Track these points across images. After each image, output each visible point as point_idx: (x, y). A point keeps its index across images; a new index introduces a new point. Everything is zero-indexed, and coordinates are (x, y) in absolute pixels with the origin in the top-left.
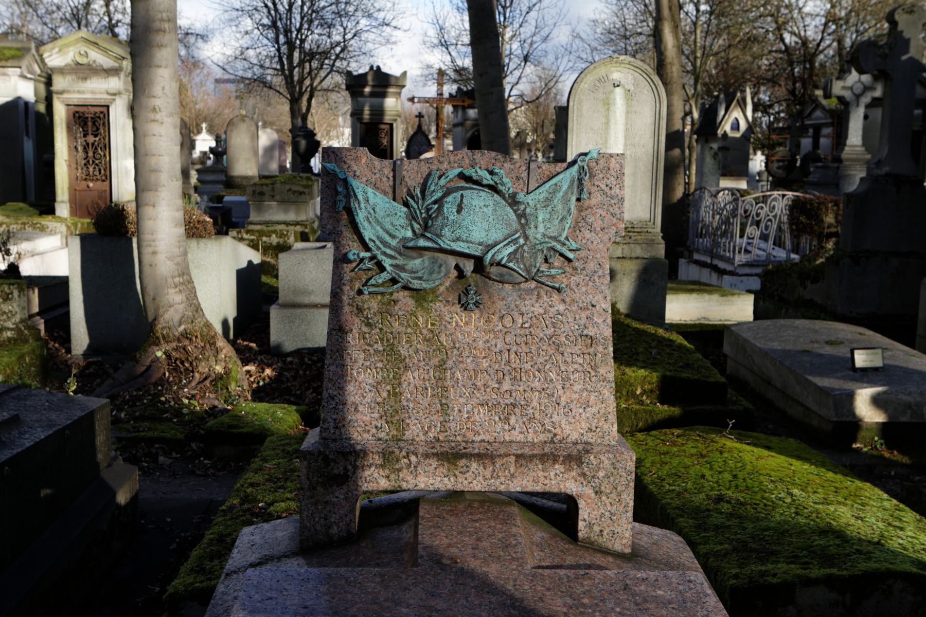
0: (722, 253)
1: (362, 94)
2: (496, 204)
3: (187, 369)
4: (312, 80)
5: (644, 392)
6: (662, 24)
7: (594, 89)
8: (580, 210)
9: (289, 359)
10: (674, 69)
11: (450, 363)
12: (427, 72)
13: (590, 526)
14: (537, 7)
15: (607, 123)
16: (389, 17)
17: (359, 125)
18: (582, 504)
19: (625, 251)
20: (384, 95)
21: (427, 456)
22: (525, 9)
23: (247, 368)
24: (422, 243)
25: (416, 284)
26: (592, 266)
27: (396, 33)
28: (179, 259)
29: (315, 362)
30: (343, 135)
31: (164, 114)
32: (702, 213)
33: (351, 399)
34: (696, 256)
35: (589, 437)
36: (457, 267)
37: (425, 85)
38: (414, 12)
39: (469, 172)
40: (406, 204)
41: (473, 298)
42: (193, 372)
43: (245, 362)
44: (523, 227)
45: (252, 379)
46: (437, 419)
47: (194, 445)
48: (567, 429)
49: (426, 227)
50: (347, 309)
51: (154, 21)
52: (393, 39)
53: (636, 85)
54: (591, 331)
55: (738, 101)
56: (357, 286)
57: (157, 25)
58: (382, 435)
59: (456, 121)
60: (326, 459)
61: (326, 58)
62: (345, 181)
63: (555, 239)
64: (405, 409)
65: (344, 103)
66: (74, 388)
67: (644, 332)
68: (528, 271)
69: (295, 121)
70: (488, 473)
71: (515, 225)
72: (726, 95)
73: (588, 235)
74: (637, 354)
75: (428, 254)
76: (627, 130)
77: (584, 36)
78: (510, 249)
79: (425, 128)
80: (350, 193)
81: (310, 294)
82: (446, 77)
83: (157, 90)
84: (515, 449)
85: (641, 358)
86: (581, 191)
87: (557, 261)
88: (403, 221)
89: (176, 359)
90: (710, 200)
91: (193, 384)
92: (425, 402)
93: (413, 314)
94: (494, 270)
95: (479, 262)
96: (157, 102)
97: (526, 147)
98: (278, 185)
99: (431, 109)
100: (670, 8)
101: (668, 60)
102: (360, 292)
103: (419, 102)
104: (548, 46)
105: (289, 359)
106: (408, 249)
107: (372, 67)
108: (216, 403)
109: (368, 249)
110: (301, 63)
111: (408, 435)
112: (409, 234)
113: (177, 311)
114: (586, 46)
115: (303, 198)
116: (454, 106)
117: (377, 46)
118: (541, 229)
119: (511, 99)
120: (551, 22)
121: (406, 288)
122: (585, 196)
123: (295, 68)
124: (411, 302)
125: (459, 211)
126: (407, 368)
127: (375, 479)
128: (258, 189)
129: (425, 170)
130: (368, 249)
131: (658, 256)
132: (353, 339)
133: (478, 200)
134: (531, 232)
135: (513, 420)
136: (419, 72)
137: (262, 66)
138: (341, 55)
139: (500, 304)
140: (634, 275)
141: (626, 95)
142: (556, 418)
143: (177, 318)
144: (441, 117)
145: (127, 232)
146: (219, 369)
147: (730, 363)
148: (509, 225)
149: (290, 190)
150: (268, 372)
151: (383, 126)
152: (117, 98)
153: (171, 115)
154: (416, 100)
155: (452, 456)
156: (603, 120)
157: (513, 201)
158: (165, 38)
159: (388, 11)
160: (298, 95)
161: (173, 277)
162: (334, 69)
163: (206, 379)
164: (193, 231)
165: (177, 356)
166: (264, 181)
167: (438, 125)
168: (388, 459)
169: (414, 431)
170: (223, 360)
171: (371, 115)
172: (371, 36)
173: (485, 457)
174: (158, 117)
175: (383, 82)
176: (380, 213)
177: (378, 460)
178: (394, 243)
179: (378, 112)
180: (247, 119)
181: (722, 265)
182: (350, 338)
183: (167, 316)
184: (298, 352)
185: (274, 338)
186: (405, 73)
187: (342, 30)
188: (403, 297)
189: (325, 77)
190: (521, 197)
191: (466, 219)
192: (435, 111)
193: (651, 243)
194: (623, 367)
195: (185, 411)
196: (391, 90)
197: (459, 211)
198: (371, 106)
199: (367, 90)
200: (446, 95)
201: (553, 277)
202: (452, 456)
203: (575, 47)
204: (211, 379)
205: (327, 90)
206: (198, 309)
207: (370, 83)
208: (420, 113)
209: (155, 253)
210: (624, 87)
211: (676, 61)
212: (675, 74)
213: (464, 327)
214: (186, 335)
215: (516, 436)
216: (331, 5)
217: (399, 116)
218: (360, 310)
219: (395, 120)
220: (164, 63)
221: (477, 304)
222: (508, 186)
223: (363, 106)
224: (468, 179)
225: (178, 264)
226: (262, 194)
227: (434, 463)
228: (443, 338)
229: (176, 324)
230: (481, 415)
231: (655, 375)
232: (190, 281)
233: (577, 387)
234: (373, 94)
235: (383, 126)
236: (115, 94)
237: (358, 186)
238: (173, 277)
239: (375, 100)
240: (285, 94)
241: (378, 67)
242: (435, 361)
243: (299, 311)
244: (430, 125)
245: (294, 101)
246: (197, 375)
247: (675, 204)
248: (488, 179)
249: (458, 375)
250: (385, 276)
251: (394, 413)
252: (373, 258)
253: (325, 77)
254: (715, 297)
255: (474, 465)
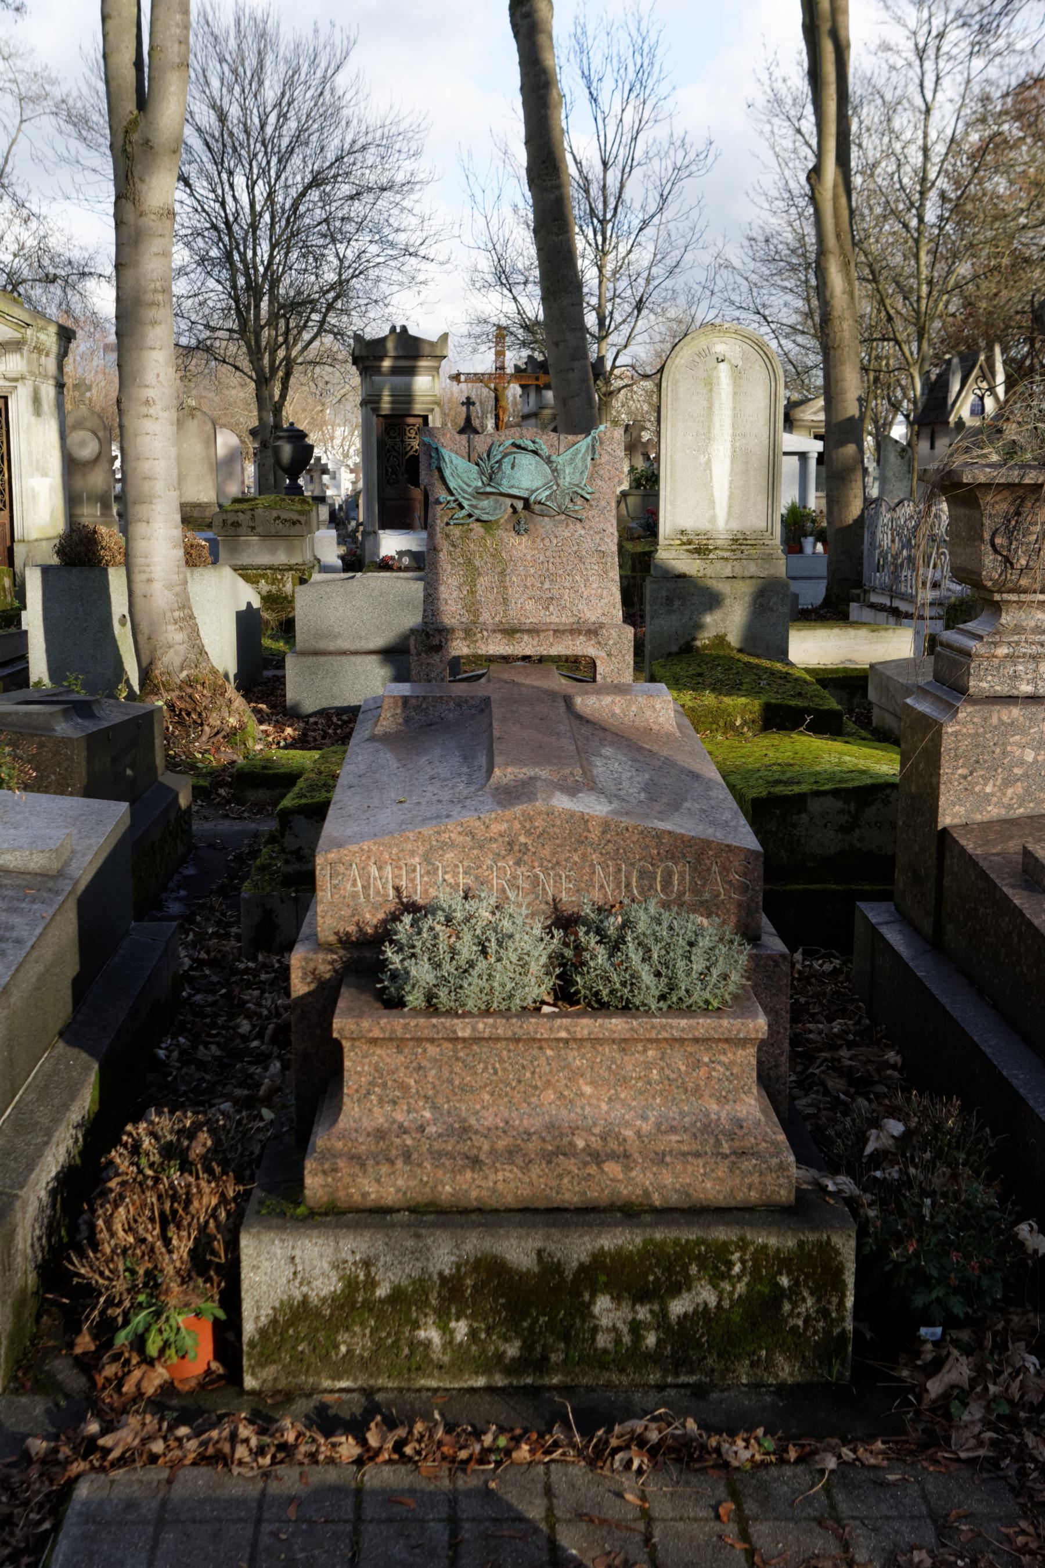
0: (903, 589)
1: (378, 371)
2: (537, 463)
3: (195, 722)
4: (288, 349)
5: (745, 723)
6: (826, 260)
7: (693, 365)
8: (594, 466)
9: (312, 720)
10: (845, 326)
11: (508, 571)
12: (477, 330)
13: (604, 678)
14: (656, 220)
15: (710, 408)
16: (415, 238)
17: (375, 419)
18: (598, 663)
19: (736, 569)
20: (412, 371)
21: (494, 631)
22: (636, 223)
23: (263, 727)
24: (489, 489)
25: (485, 517)
26: (603, 504)
27: (424, 265)
28: (178, 589)
29: (345, 722)
30: (332, 438)
31: (159, 407)
32: (879, 536)
33: (443, 596)
34: (874, 598)
35: (603, 619)
36: (512, 506)
37: (475, 351)
38: (456, 232)
39: (519, 442)
40: (477, 464)
41: (523, 526)
42: (202, 725)
43: (261, 723)
44: (556, 478)
45: (270, 739)
46: (501, 608)
47: (222, 791)
48: (588, 614)
49: (491, 479)
50: (439, 535)
51: (145, 292)
52: (421, 277)
53: (745, 359)
54: (603, 548)
55: (981, 367)
56: (446, 520)
57: (149, 297)
58: (464, 620)
59: (526, 410)
60: (427, 635)
61: (313, 311)
62: (437, 449)
63: (577, 485)
64: (479, 602)
65: (349, 381)
66: (124, 694)
67: (758, 667)
68: (560, 507)
69: (265, 415)
70: (535, 643)
71: (550, 477)
72: (963, 358)
73: (600, 483)
74: (741, 684)
75: (493, 497)
76: (735, 416)
77: (736, 263)
78: (547, 493)
79: (476, 423)
80: (440, 457)
81: (336, 637)
82: (509, 340)
83: (150, 377)
84: (553, 627)
85: (744, 687)
86: (594, 453)
87: (579, 501)
88: (476, 476)
89: (181, 710)
90: (889, 516)
91: (204, 738)
92: (492, 597)
93: (483, 538)
94: (537, 508)
95: (526, 501)
96: (151, 393)
97: (640, 450)
98: (259, 511)
99: (485, 391)
100: (838, 236)
101: (836, 313)
102: (448, 524)
103: (466, 381)
104: (678, 282)
105: (312, 720)
106: (480, 494)
107: (393, 329)
108: (235, 757)
109: (452, 494)
110: (274, 317)
111: (481, 619)
112: (480, 484)
113: (177, 652)
114: (740, 280)
115: (297, 530)
116: (522, 386)
117: (395, 288)
118: (568, 479)
119: (616, 372)
120: (682, 242)
121: (478, 520)
122: (596, 456)
123: (262, 327)
124: (481, 531)
125: (513, 467)
126: (479, 574)
127: (459, 648)
128: (231, 518)
129: (489, 442)
130: (452, 494)
131: (778, 575)
132: (443, 556)
133: (526, 460)
134: (561, 482)
135: (551, 608)
136: (465, 329)
137: (207, 326)
138: (339, 305)
139: (542, 531)
140: (747, 598)
141: (733, 372)
142: (580, 607)
143: (178, 662)
144: (502, 403)
145: (100, 562)
146: (233, 721)
147: (876, 712)
148: (546, 476)
149: (278, 518)
150: (289, 731)
151: (411, 420)
152: (19, 384)
153: (166, 409)
154: (463, 378)
155: (510, 632)
156: (705, 404)
157: (549, 461)
158: (161, 313)
159: (414, 231)
160: (270, 378)
161: (172, 611)
162: (326, 327)
163: (218, 733)
164: (192, 559)
165: (182, 706)
166: (237, 506)
167: (497, 417)
168: (468, 633)
169: (485, 617)
170: (236, 711)
171: (392, 402)
172: (385, 273)
173: (533, 631)
174: (152, 411)
175: (410, 350)
176: (460, 470)
177: (462, 635)
178: (470, 490)
179: (404, 398)
180: (198, 413)
181: (904, 607)
182: (441, 555)
183: (165, 659)
184: (322, 713)
185: (291, 695)
186: (445, 337)
187: (336, 262)
188: (477, 527)
189: (310, 342)
190: (554, 458)
191: (518, 473)
192: (493, 394)
193: (768, 558)
194: (721, 697)
195: (200, 765)
196: (423, 363)
197: (513, 467)
198: (392, 389)
199: (387, 363)
200: (510, 370)
201: (576, 511)
202: (510, 632)
203: (720, 283)
204: (224, 733)
205: (313, 363)
206: (202, 651)
207: (392, 353)
208: (468, 398)
209: (149, 581)
210: (730, 362)
211: (847, 314)
212: (847, 334)
213: (518, 546)
214: (189, 682)
215: (554, 619)
216: (319, 224)
217: (437, 403)
218: (448, 536)
219: (432, 410)
220: (158, 344)
221: (526, 531)
222: (545, 451)
223: (381, 390)
224: (519, 447)
225: (177, 595)
226: (236, 525)
227: (499, 636)
228: (504, 554)
229: (177, 669)
230: (530, 605)
231: (757, 702)
232: (192, 617)
233: (594, 586)
234: (395, 371)
235: (411, 420)
236: (16, 380)
237: (446, 453)
238: (172, 611)
239: (399, 380)
240: (246, 370)
241: (404, 329)
242: (499, 570)
243: (323, 659)
244: (484, 417)
245: (262, 382)
246: (207, 729)
247: (850, 526)
248: (531, 446)
249: (514, 578)
250: (464, 513)
251: (472, 607)
252: (456, 500)
253: (310, 342)
254: (863, 632)
255: (526, 637)
